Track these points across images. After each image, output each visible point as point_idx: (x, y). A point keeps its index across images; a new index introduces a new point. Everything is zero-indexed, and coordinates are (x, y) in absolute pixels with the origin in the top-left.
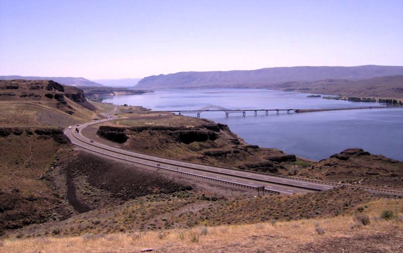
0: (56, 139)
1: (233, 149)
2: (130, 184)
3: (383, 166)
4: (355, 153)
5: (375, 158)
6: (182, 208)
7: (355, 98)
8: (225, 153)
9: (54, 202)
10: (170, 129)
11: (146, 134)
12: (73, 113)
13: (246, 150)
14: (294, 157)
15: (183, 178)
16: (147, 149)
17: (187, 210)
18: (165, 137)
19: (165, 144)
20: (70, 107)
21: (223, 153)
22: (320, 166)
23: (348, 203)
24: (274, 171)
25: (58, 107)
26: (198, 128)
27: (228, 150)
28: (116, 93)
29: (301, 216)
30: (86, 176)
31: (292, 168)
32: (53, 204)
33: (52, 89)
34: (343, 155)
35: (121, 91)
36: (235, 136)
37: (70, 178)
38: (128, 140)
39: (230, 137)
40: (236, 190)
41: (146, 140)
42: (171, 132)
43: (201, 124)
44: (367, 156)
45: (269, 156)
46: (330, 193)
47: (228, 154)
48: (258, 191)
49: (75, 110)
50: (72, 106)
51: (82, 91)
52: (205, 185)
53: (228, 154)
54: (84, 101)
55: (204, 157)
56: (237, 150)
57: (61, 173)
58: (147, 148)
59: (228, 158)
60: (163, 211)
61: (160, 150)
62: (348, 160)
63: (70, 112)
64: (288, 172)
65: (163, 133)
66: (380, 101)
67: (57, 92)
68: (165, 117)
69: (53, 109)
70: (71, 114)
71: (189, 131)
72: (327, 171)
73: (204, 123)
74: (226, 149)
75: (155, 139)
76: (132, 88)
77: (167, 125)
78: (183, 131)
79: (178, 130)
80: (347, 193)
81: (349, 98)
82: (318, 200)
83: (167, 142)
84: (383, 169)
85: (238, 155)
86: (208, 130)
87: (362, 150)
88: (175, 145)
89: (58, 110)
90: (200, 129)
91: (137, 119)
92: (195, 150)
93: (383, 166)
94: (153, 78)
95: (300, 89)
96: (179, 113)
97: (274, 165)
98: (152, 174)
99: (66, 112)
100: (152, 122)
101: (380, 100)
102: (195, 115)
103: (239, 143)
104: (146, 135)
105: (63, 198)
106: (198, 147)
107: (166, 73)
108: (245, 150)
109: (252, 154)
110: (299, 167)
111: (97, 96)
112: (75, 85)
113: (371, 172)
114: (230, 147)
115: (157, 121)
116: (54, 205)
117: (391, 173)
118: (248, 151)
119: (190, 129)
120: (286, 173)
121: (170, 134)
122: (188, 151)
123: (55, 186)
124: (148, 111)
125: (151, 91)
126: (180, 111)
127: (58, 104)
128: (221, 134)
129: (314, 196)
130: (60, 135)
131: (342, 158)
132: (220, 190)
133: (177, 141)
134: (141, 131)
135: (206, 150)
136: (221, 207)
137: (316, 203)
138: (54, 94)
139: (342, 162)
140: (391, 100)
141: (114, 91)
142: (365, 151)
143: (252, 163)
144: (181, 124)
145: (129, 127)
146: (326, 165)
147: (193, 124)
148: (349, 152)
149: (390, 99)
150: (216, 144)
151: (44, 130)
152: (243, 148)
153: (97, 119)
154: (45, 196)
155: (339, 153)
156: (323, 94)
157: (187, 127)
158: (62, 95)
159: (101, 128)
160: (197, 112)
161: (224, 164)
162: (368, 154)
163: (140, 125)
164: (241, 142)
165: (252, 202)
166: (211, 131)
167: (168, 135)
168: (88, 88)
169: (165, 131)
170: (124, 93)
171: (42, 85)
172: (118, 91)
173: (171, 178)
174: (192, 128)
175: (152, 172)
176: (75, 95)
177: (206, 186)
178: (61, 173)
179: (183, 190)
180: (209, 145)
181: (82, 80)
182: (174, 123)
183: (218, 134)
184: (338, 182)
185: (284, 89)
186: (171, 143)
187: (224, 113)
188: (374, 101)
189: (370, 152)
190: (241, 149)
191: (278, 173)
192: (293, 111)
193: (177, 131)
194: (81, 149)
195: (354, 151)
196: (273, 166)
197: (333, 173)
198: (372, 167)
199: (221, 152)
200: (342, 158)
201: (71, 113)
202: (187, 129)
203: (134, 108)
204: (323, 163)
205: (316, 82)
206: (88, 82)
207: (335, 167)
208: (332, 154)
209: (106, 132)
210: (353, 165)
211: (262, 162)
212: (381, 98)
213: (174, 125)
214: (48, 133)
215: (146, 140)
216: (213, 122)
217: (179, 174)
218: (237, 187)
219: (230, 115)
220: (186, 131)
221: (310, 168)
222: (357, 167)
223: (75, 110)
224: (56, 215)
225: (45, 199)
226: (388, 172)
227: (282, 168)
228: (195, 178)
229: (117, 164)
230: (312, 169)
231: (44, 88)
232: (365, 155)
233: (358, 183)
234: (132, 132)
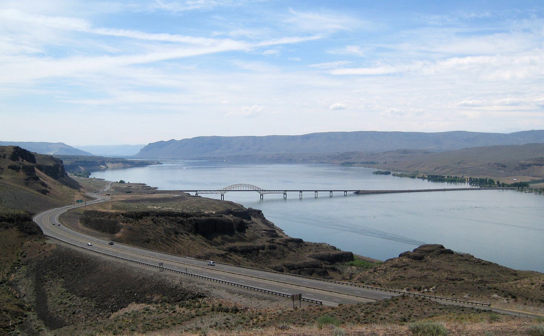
0: (21, 229)
1: (267, 244)
2: (121, 290)
3: (470, 269)
4: (433, 251)
5: (460, 258)
6: (188, 322)
7: (437, 176)
8: (258, 249)
9: (15, 315)
10: (183, 215)
11: (148, 221)
12: (48, 192)
13: (285, 245)
15: (193, 282)
16: (148, 242)
17: (193, 324)
18: (173, 227)
19: (173, 236)
20: (44, 185)
22: (385, 268)
23: (407, 317)
24: (324, 274)
25: (27, 184)
26: (219, 214)
27: (261, 245)
28: (109, 165)
30: (62, 280)
31: (348, 270)
32: (16, 317)
33: (18, 159)
34: (417, 254)
35: (117, 162)
36: (271, 225)
37: (40, 282)
39: (264, 227)
40: (265, 299)
41: (148, 230)
42: (181, 219)
43: (225, 209)
45: (317, 254)
46: (385, 303)
47: (260, 251)
48: (293, 300)
49: (50, 188)
50: (46, 182)
51: (62, 162)
52: (224, 291)
53: (260, 251)
54: (64, 174)
55: (226, 254)
56: (272, 244)
57: (27, 276)
58: (148, 241)
59: (260, 255)
60: (160, 326)
61: (167, 244)
62: (423, 260)
63: (44, 190)
64: (342, 276)
65: (171, 221)
66: (472, 182)
67: (26, 163)
68: (174, 199)
69: (19, 186)
70: (45, 194)
71: (207, 218)
72: (393, 274)
73: (229, 207)
74: (258, 243)
75: (160, 229)
76: (132, 157)
77: (179, 210)
78: (199, 218)
79: (192, 216)
80: (408, 303)
81: (429, 176)
82: (368, 313)
83: (176, 233)
84: (469, 273)
86: (235, 218)
87: (442, 247)
88: (187, 238)
89: (27, 189)
90: (224, 215)
91: (137, 201)
92: (217, 244)
93: (470, 269)
94: (161, 145)
95: (363, 163)
96: (195, 193)
97: (324, 266)
98: (152, 277)
99: (38, 191)
100: (157, 206)
101: (470, 179)
102: (218, 197)
103: (277, 236)
104: (148, 223)
105: (29, 310)
107: (178, 138)
108: (284, 245)
109: (294, 251)
110: (357, 269)
111: (82, 169)
112: (52, 154)
113: (453, 277)
114: (263, 241)
115: (164, 204)
116: (17, 319)
117: (479, 279)
118: (288, 246)
119: (208, 215)
120: (339, 277)
121: (181, 222)
122: (206, 246)
123: (20, 293)
124: (154, 190)
125: (158, 163)
126: (197, 191)
127: (28, 180)
128: (253, 223)
129: (363, 308)
130: (28, 223)
132: (244, 299)
133: (190, 232)
134: (141, 218)
136: (242, 321)
137: (365, 317)
138: (21, 166)
139: (414, 263)
140: (486, 180)
141: (107, 162)
142: (447, 247)
143: (292, 262)
144: (198, 208)
145: (123, 212)
146: (393, 266)
147: (215, 209)
148: (424, 249)
149: (484, 177)
151: (4, 216)
152: (281, 242)
153: (81, 201)
154: (5, 307)
155: (412, 251)
156: (393, 170)
157: (206, 212)
158: (33, 167)
159: (87, 213)
160: (220, 192)
161: (253, 264)
162: (450, 252)
163: (141, 210)
164: (280, 234)
165: (283, 314)
166: (238, 219)
167: (178, 223)
168: (70, 158)
169: (174, 218)
170: (120, 165)
171: (5, 153)
172: (113, 163)
173: (177, 282)
174: (212, 214)
175: (152, 274)
176: (50, 167)
177: (223, 293)
178: (27, 276)
179: (193, 298)
181: (63, 147)
182: (188, 207)
183: (249, 222)
184: (402, 289)
185: (340, 162)
186: (182, 234)
187: (257, 194)
188: (463, 181)
189: (452, 249)
190: (279, 244)
191: (328, 277)
193: (191, 218)
194: (57, 242)
195: (432, 248)
196: (322, 267)
197: (401, 277)
198: (455, 270)
199: (250, 247)
201: (45, 192)
202: (205, 215)
203: (134, 187)
204: (389, 265)
205: (385, 153)
206: (69, 148)
207: (405, 269)
208: (403, 251)
209: (93, 219)
210: (429, 267)
211: (307, 261)
212: (473, 177)
213: (187, 209)
214: (10, 220)
215: (148, 230)
216: (242, 206)
217: (189, 277)
218: (266, 295)
220: (203, 218)
221: (372, 270)
222: (434, 270)
223: (50, 188)
224: (19, 333)
225: (5, 310)
226: (476, 277)
227: (334, 270)
228: (208, 282)
229: (105, 262)
230: (375, 271)
231: (7, 157)
232: (446, 253)
233: (428, 292)
234: (128, 218)
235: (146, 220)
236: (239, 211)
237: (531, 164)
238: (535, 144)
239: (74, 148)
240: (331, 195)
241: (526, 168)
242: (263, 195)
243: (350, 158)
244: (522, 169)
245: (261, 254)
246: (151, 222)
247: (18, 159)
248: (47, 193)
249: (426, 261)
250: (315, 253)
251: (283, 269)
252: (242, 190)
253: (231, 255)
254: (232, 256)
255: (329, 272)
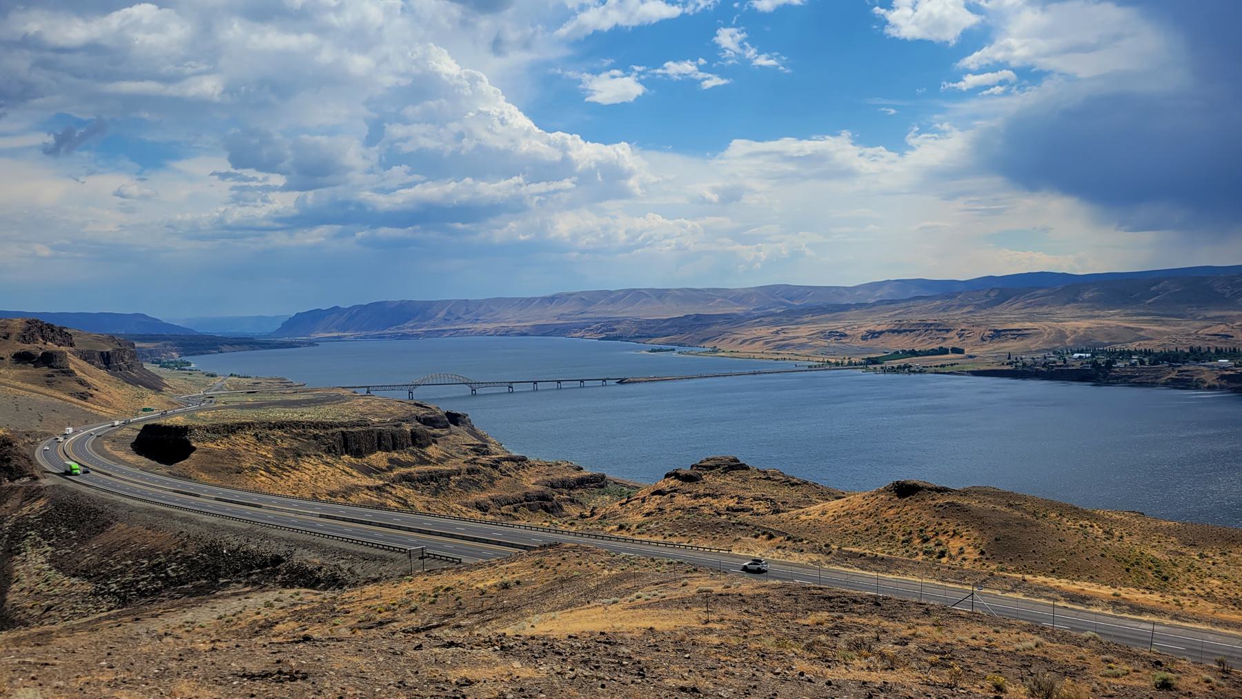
1: (465, 467)
4: (718, 466)
14: (603, 477)
19: (291, 462)
20: (82, 383)
21: (442, 476)
22: (642, 496)
25: (49, 384)
27: (455, 468)
29: (1053, 572)
38: (193, 455)
44: (741, 472)
45: (549, 478)
50: (88, 379)
56: (473, 466)
78: (350, 430)
85: (477, 477)
99: (71, 394)
106: (384, 464)
107: (345, 304)
108: (493, 467)
131: (688, 479)
134: (233, 432)
135: (403, 471)
139: (687, 486)
144: (362, 413)
148: (708, 464)
150: (429, 456)
180: (411, 458)
192: (613, 382)
193: (335, 430)
198: (748, 494)
200: (688, 479)
201: (83, 397)
207: (672, 497)
219: (516, 387)
231: (13, 337)
235: (245, 436)
236: (430, 416)
237: (884, 330)
238: (275, 317)
239: (165, 322)
240: (559, 387)
241: (877, 337)
242: (475, 391)
243: (614, 330)
244: (871, 338)
245: (454, 482)
246: (254, 439)
247: (35, 341)
248: (90, 398)
249: (704, 483)
250: (546, 478)
251: (489, 505)
252: (439, 383)
253: (393, 487)
254: (395, 488)
255: (564, 506)
